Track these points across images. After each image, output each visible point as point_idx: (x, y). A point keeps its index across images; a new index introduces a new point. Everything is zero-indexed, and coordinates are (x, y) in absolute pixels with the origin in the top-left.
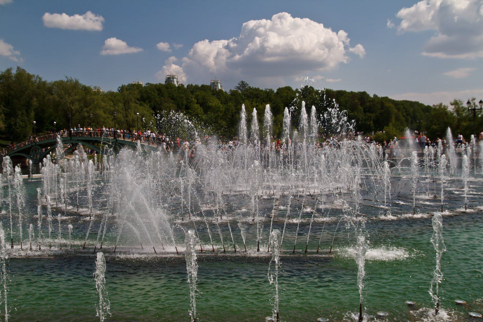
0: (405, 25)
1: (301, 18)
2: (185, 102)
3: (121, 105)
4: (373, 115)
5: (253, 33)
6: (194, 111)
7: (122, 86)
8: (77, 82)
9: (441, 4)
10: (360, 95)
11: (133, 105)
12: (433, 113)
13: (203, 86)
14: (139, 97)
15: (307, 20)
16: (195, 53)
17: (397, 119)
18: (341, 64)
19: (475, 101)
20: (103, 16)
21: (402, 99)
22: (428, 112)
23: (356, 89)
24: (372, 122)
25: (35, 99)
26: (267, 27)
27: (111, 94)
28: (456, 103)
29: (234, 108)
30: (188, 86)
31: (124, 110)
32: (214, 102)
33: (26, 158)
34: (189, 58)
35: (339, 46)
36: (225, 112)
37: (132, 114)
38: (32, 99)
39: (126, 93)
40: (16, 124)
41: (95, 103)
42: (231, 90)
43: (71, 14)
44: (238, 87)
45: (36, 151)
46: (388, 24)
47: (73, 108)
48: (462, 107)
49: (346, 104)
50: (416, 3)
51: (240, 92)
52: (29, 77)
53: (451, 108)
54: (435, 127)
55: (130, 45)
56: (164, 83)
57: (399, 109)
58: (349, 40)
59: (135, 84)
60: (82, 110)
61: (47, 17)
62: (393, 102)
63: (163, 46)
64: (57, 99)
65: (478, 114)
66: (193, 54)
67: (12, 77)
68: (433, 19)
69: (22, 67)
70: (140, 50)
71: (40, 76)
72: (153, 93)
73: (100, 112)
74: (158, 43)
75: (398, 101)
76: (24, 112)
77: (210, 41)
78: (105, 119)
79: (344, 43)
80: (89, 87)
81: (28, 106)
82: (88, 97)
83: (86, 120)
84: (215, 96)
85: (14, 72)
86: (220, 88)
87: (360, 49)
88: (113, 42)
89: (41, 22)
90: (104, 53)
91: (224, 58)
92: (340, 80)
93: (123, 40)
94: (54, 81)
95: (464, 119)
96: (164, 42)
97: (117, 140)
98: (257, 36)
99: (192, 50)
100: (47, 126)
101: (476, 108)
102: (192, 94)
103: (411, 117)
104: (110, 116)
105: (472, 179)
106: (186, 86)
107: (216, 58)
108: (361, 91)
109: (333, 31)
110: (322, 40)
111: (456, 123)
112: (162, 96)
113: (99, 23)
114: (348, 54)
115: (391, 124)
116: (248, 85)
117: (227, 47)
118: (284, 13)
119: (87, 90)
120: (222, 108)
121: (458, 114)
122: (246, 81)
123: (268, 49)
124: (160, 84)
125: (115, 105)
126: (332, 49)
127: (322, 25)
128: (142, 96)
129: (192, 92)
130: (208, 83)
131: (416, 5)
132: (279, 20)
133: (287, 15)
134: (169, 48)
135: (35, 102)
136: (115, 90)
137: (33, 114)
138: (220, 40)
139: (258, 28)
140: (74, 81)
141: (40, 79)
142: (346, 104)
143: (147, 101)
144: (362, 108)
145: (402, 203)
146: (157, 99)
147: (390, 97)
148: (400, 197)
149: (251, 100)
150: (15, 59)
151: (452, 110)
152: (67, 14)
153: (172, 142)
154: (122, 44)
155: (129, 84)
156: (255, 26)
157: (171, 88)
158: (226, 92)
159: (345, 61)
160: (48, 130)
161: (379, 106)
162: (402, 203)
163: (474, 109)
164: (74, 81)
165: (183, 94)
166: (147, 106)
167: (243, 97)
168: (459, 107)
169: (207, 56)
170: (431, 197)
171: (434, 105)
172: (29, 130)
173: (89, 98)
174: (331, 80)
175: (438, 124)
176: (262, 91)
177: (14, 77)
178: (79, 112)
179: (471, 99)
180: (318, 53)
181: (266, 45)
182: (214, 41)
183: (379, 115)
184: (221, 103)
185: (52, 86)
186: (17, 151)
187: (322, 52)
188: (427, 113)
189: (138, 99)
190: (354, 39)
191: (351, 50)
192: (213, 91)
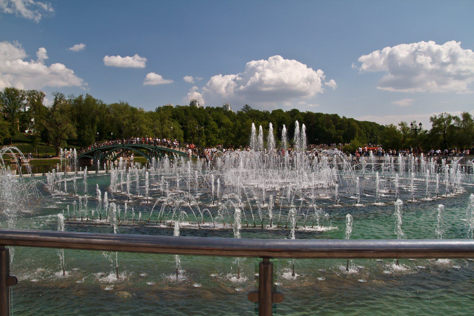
0: (364, 67)
1: (290, 60)
2: (204, 120)
3: (158, 121)
4: (343, 131)
5: (254, 70)
6: (211, 127)
7: (159, 107)
8: (127, 105)
9: (389, 54)
10: (333, 117)
11: (167, 121)
12: (386, 131)
13: (217, 108)
14: (171, 116)
15: (294, 61)
16: (211, 84)
17: (360, 134)
18: (319, 94)
19: (416, 123)
20: (146, 58)
21: (363, 120)
22: (382, 130)
23: (330, 113)
24: (341, 137)
25: (98, 117)
26: (265, 66)
27: (151, 113)
28: (402, 124)
29: (240, 124)
30: (206, 108)
31: (160, 125)
32: (226, 120)
33: (91, 159)
34: (207, 88)
35: (318, 81)
36: (233, 127)
37: (166, 128)
38: (95, 117)
39: (162, 112)
40: (84, 135)
41: (140, 119)
42: (238, 111)
43: (123, 56)
44: (243, 109)
45: (98, 154)
46: (352, 66)
47: (124, 123)
48: (407, 127)
49: (323, 123)
50: (372, 52)
51: (244, 112)
52: (94, 101)
53: (399, 128)
54: (387, 141)
55: (164, 77)
56: (189, 106)
57: (361, 128)
58: (325, 76)
59: (168, 106)
60: (130, 124)
61: (107, 59)
62: (357, 122)
63: (188, 79)
64: (113, 116)
65: (418, 133)
66: (210, 85)
67: (82, 101)
68: (384, 64)
69: (90, 94)
70: (172, 81)
71: (102, 100)
72: (181, 112)
73: (144, 126)
74: (185, 76)
75: (360, 122)
76: (90, 126)
77: (223, 76)
78: (147, 131)
79: (321, 78)
80: (136, 108)
81: (93, 121)
82: (135, 115)
83: (133, 132)
84: (226, 115)
85: (84, 98)
86: (230, 110)
87: (333, 82)
88: (152, 76)
89: (102, 62)
90: (145, 83)
91: (232, 88)
92: (318, 105)
93: (160, 75)
94: (111, 104)
95: (408, 136)
96: (189, 76)
97: (156, 147)
98: (257, 72)
99: (209, 82)
100: (105, 136)
101: (417, 128)
102: (210, 114)
103: (370, 133)
104: (150, 129)
105: (416, 179)
106: (205, 108)
107: (226, 88)
108: (334, 114)
109: (314, 70)
110: (305, 76)
111: (402, 138)
112: (187, 115)
113: (144, 63)
114: (323, 86)
115: (356, 138)
116: (250, 108)
117: (235, 80)
118: (277, 56)
119: (133, 110)
120: (231, 124)
121: (404, 132)
122: (250, 105)
123: (265, 82)
124: (186, 106)
125: (154, 121)
126: (313, 83)
127: (306, 66)
128: (173, 115)
129: (210, 112)
130: (221, 106)
131: (372, 53)
132: (274, 60)
133: (280, 57)
134: (193, 80)
135: (98, 119)
136: (154, 110)
137: (96, 127)
138: (230, 75)
139: (258, 66)
140: (125, 103)
141: (102, 102)
142: (323, 123)
143: (176, 119)
144: (334, 126)
145: (367, 195)
146: (184, 117)
147: (355, 119)
148: (366, 191)
149: (253, 118)
150: (84, 89)
151: (399, 129)
152: (121, 56)
153: (197, 149)
154: (159, 77)
155: (164, 106)
156: (255, 65)
157: (194, 109)
158: (234, 113)
159: (322, 92)
160: (105, 139)
161: (347, 125)
162: (367, 195)
163: (416, 129)
164: (125, 103)
165: (203, 113)
166: (177, 122)
167: (247, 117)
168: (404, 127)
169: (220, 86)
170: (387, 191)
171: (386, 125)
172: (93, 138)
173: (136, 116)
174: (311, 105)
175: (390, 139)
176: (261, 112)
177: (84, 101)
178: (128, 126)
179: (413, 122)
180: (302, 85)
181: (264, 78)
182: (226, 76)
183: (347, 131)
184: (231, 121)
185: (110, 107)
186: (85, 154)
187: (305, 84)
188: (382, 131)
189: (171, 117)
190: (328, 75)
191: (326, 83)
192: (225, 112)
